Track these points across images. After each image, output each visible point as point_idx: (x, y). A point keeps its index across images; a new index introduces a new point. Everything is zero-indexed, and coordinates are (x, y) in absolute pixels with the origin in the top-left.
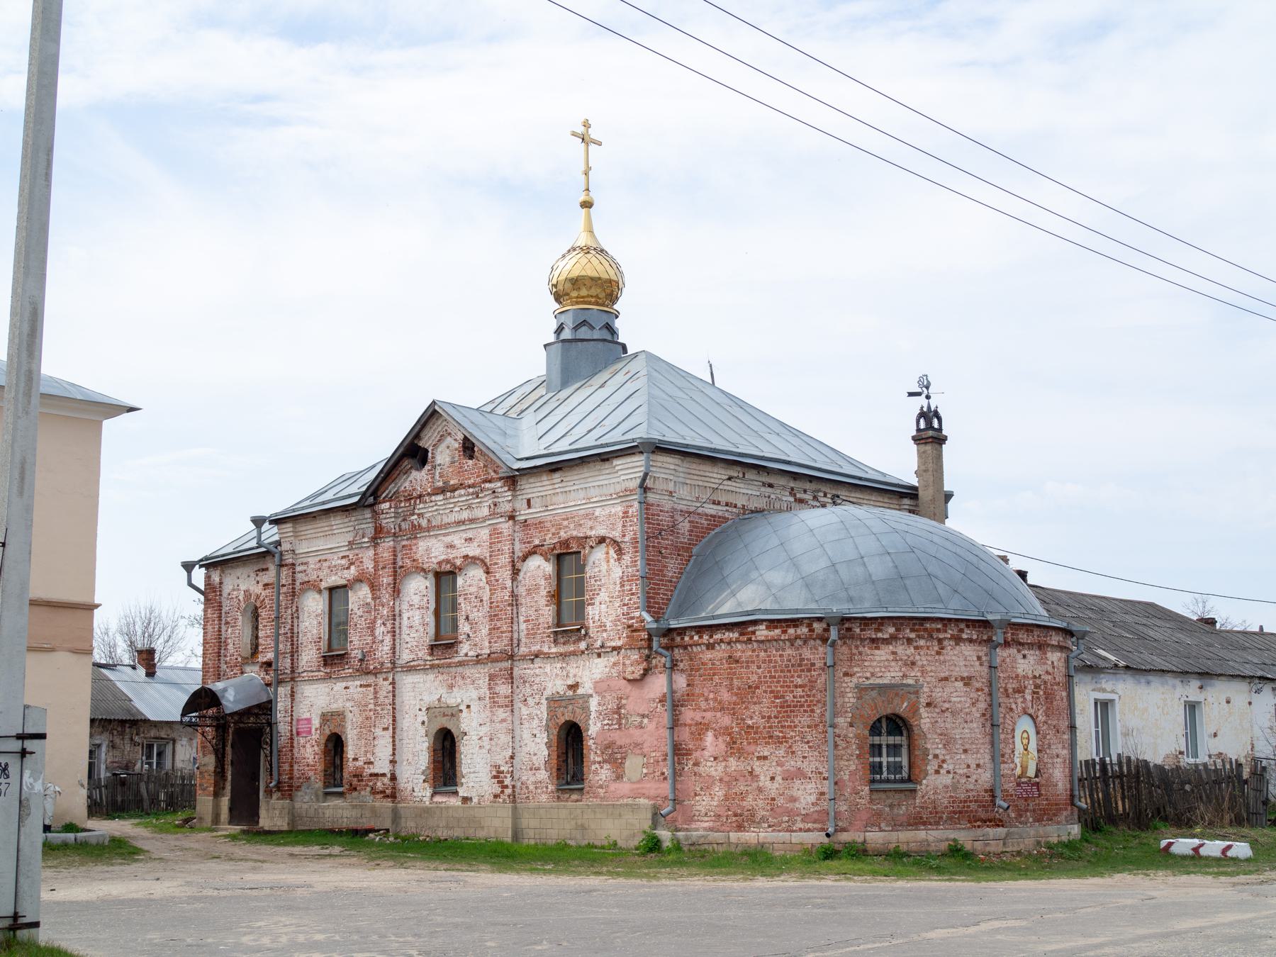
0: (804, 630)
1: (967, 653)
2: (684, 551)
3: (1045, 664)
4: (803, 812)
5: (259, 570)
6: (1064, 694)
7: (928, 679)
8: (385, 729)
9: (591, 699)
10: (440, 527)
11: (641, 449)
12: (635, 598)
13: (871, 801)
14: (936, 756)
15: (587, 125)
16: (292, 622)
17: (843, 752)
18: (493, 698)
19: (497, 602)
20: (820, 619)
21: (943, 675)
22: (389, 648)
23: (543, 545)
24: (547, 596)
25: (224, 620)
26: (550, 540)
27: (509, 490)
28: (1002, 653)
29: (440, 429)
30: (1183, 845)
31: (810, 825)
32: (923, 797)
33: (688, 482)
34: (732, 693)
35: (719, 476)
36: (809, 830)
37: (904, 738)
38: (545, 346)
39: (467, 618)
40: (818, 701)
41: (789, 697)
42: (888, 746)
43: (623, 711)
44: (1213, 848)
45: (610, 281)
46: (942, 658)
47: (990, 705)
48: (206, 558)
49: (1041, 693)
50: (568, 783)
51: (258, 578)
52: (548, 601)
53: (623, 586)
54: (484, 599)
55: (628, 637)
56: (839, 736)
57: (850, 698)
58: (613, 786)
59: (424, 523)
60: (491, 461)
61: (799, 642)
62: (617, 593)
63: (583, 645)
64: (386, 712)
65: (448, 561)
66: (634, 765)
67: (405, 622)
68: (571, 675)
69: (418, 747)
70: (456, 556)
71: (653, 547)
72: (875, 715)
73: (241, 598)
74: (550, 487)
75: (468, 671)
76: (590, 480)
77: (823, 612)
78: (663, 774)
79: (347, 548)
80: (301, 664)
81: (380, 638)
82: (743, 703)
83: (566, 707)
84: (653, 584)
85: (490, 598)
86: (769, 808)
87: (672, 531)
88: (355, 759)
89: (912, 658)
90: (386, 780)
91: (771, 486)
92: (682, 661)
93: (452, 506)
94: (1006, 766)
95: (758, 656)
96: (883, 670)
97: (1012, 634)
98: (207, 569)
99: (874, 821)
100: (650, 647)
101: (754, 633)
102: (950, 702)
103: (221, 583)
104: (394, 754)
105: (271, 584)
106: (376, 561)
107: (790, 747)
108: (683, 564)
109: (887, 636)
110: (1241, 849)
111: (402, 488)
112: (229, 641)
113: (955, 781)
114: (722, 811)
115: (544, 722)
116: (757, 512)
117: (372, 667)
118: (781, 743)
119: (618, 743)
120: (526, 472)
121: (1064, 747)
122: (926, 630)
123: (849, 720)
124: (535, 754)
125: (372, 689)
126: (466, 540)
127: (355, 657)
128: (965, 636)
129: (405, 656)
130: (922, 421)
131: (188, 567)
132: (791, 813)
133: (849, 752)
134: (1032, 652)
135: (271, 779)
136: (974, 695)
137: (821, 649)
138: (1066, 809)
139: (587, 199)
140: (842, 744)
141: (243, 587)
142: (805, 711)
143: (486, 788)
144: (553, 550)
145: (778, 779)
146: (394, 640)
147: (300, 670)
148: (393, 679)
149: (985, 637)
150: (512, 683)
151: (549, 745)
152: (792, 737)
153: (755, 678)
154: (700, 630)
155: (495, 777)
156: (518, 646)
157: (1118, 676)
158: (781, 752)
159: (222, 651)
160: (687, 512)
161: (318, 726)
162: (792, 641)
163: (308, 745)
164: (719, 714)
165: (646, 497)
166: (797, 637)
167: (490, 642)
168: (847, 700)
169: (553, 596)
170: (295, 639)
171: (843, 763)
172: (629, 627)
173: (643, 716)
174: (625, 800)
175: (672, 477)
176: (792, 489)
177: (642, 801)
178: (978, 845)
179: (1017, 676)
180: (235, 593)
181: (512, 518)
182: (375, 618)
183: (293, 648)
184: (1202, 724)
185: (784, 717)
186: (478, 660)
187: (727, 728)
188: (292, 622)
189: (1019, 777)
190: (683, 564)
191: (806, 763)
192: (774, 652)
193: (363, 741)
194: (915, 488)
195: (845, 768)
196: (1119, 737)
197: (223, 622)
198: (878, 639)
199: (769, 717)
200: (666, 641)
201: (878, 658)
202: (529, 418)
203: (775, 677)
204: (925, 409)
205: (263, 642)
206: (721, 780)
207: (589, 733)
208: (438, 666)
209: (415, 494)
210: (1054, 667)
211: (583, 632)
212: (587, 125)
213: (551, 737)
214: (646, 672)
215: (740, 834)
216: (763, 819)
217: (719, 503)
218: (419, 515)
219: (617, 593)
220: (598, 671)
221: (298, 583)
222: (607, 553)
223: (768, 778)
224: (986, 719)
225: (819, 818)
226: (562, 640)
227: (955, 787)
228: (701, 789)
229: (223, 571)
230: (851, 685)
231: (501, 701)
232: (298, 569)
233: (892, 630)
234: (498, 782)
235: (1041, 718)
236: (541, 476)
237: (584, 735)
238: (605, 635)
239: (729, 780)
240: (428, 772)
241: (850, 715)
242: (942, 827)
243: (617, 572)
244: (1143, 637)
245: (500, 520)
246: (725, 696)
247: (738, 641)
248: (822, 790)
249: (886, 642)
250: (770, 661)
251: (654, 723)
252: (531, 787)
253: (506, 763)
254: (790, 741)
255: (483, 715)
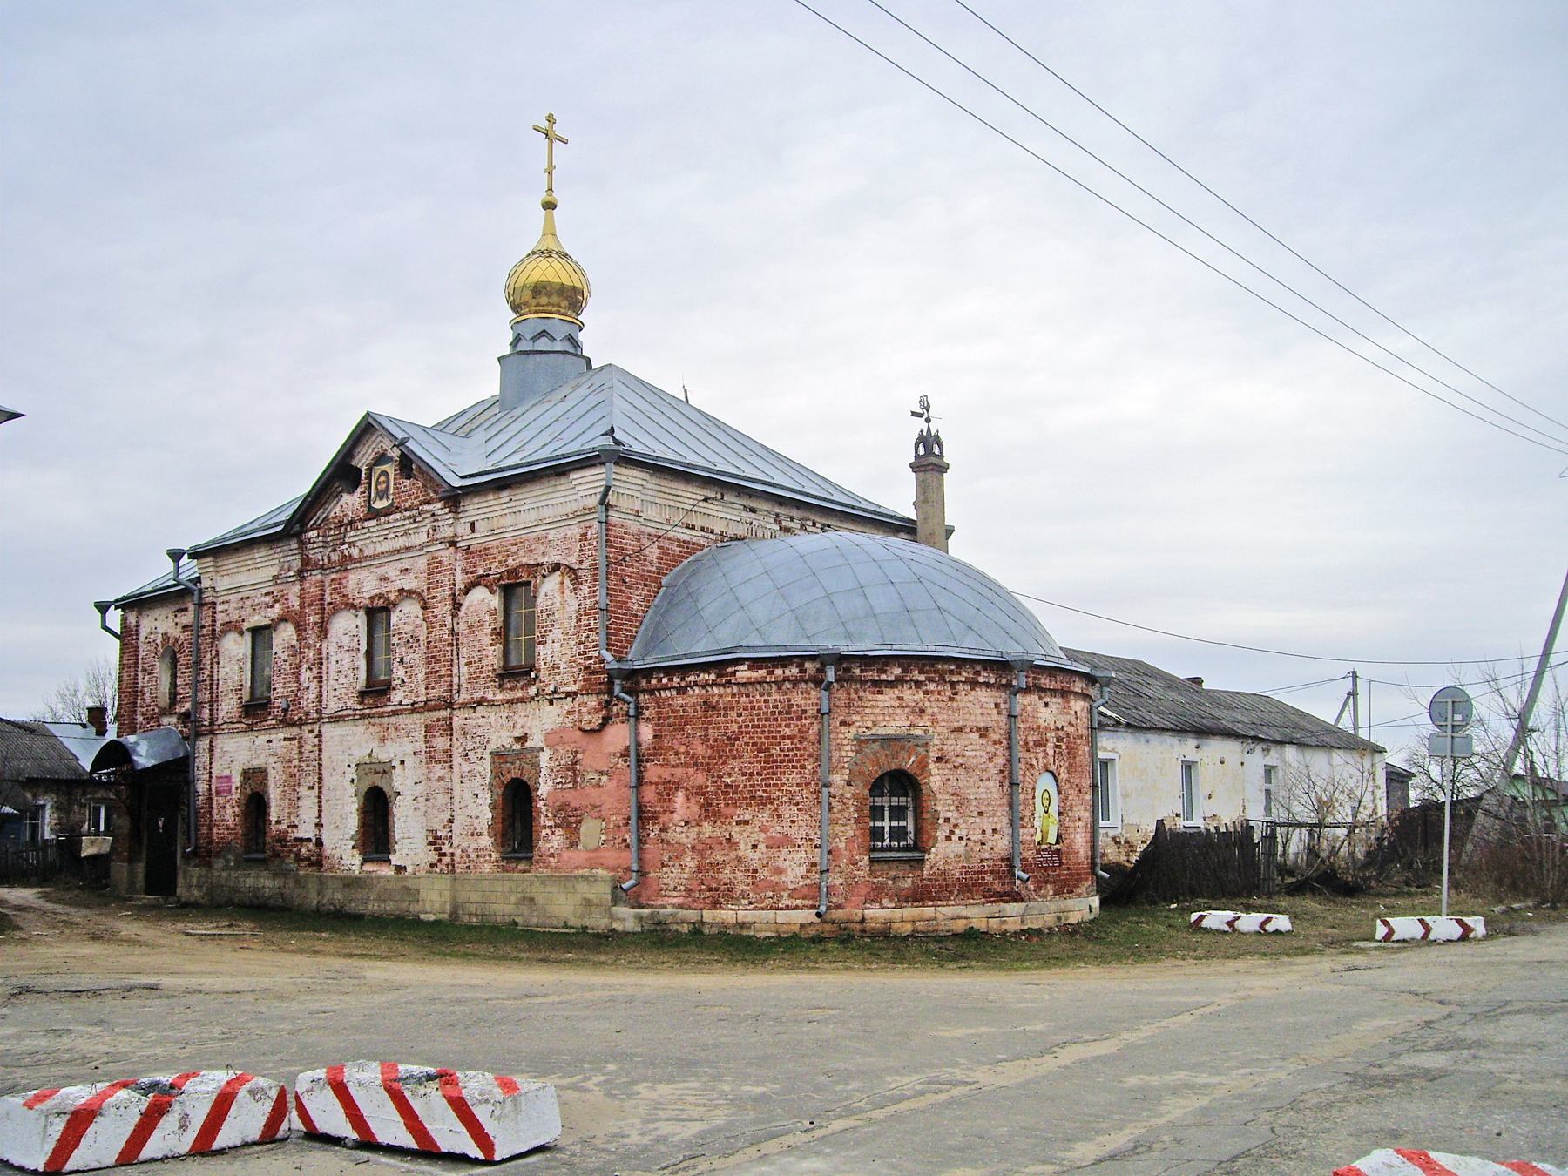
0: (793, 671)
1: (983, 700)
2: (651, 582)
3: (1068, 714)
4: (791, 886)
5: (177, 611)
6: (1087, 749)
7: (939, 729)
8: (311, 788)
9: (541, 753)
10: (372, 557)
11: (603, 459)
12: (593, 635)
13: (871, 873)
14: (947, 820)
15: (551, 119)
16: (212, 668)
17: (839, 815)
18: (430, 752)
19: (435, 642)
20: (812, 658)
21: (956, 725)
22: (315, 696)
23: (488, 575)
24: (492, 635)
25: (140, 666)
26: (497, 569)
27: (450, 512)
28: (1022, 700)
29: (374, 446)
30: (1216, 919)
31: (799, 902)
32: (932, 867)
33: (658, 501)
34: (707, 746)
35: (694, 496)
36: (796, 908)
37: (909, 799)
38: (499, 359)
39: (402, 661)
40: (810, 755)
41: (775, 751)
42: (890, 807)
43: (578, 767)
44: (1250, 921)
45: (574, 288)
46: (955, 704)
47: (1009, 761)
48: (123, 599)
49: (1064, 747)
50: (514, 851)
51: (177, 620)
52: (493, 640)
53: (580, 620)
54: (421, 638)
55: (584, 680)
56: (834, 797)
57: (848, 752)
58: (566, 855)
59: (355, 553)
60: (430, 478)
61: (788, 685)
62: (572, 629)
63: (533, 691)
64: (311, 768)
65: (380, 596)
66: (591, 831)
67: (333, 667)
68: (519, 726)
69: (347, 809)
70: (391, 589)
71: (616, 574)
72: (876, 771)
73: (159, 642)
74: (498, 508)
75: (403, 720)
76: (542, 498)
77: (816, 649)
78: (625, 840)
79: (270, 584)
80: (221, 715)
81: (306, 685)
82: (720, 757)
83: (512, 763)
84: (616, 618)
85: (428, 637)
86: (750, 881)
87: (637, 557)
88: (279, 822)
89: (920, 705)
90: (311, 846)
91: (753, 511)
92: (647, 708)
93: (386, 532)
94: (1026, 830)
95: (738, 702)
96: (887, 718)
97: (1034, 678)
98: (123, 611)
99: (876, 895)
100: (610, 692)
101: (734, 674)
102: (963, 756)
103: (138, 626)
104: (320, 817)
105: (191, 626)
106: (301, 597)
107: (776, 809)
108: (651, 596)
109: (891, 678)
110: (1282, 922)
111: (332, 514)
112: (146, 689)
113: (969, 848)
114: (694, 885)
115: (488, 780)
116: (737, 539)
117: (296, 718)
118: (765, 805)
119: (573, 804)
120: (468, 490)
121: (1085, 810)
122: (936, 672)
123: (846, 777)
124: (477, 817)
125: (296, 742)
126: (401, 571)
127: (279, 707)
128: (981, 680)
129: (332, 706)
130: (921, 447)
131: (103, 608)
132: (776, 888)
133: (846, 815)
134: (1054, 700)
135: (189, 843)
136: (991, 749)
137: (813, 693)
138: (1087, 880)
139: (549, 199)
140: (837, 806)
141: (161, 631)
142: (794, 767)
143: (422, 856)
144: (499, 580)
145: (762, 847)
146: (321, 687)
147: (220, 722)
148: (320, 731)
149: (1004, 681)
150: (452, 735)
151: (493, 807)
152: (778, 798)
153: (735, 727)
154: (669, 671)
155: (431, 843)
156: (459, 692)
157: (1119, 734)
158: (766, 816)
159: (139, 702)
160: (655, 536)
161: (239, 784)
162: (779, 684)
163: (228, 806)
164: (691, 771)
165: (607, 516)
166: (786, 679)
167: (427, 688)
168: (844, 754)
169: (499, 634)
170: (215, 687)
171: (838, 828)
172: (586, 668)
173: (602, 773)
174: (581, 871)
175: (638, 494)
176: (777, 515)
177: (600, 872)
178: (994, 923)
179: (1039, 727)
180: (152, 636)
181: (453, 544)
182: (300, 661)
183: (212, 697)
184: (1197, 780)
185: (768, 773)
186: (414, 709)
187: (700, 787)
188: (212, 668)
189: (1039, 844)
190: (651, 596)
191: (795, 828)
192: (758, 697)
193: (287, 801)
194: (914, 522)
195: (841, 834)
196: (1119, 800)
197: (140, 669)
198: (881, 682)
199: (752, 774)
200: (628, 685)
201: (881, 704)
202: (480, 436)
203: (758, 726)
204: (925, 433)
205: (182, 691)
206: (693, 848)
207: (539, 793)
208: (369, 716)
209: (346, 521)
210: (1077, 718)
211: (533, 675)
212: (551, 119)
213: (495, 797)
214: (606, 721)
215: (716, 912)
216: (744, 895)
217: (693, 528)
218: (349, 544)
219: (572, 629)
220: (549, 720)
221: (218, 624)
222: (562, 583)
223: (749, 847)
224: (1004, 777)
225: (812, 894)
226: (508, 686)
227: (968, 857)
228: (670, 859)
229: (140, 613)
230: (850, 736)
231: (439, 755)
232: (219, 608)
233: (897, 671)
234: (435, 849)
235: (1063, 776)
236: (486, 495)
237: (534, 794)
238: (558, 678)
239: (702, 849)
240: (357, 837)
241: (848, 771)
242: (952, 903)
243: (573, 605)
244: (1138, 695)
245: (440, 547)
246: (700, 749)
247: (714, 684)
248: (813, 860)
249: (892, 684)
250: (753, 708)
251: (615, 781)
252: (473, 856)
253: (444, 827)
254: (776, 802)
255: (419, 771)
